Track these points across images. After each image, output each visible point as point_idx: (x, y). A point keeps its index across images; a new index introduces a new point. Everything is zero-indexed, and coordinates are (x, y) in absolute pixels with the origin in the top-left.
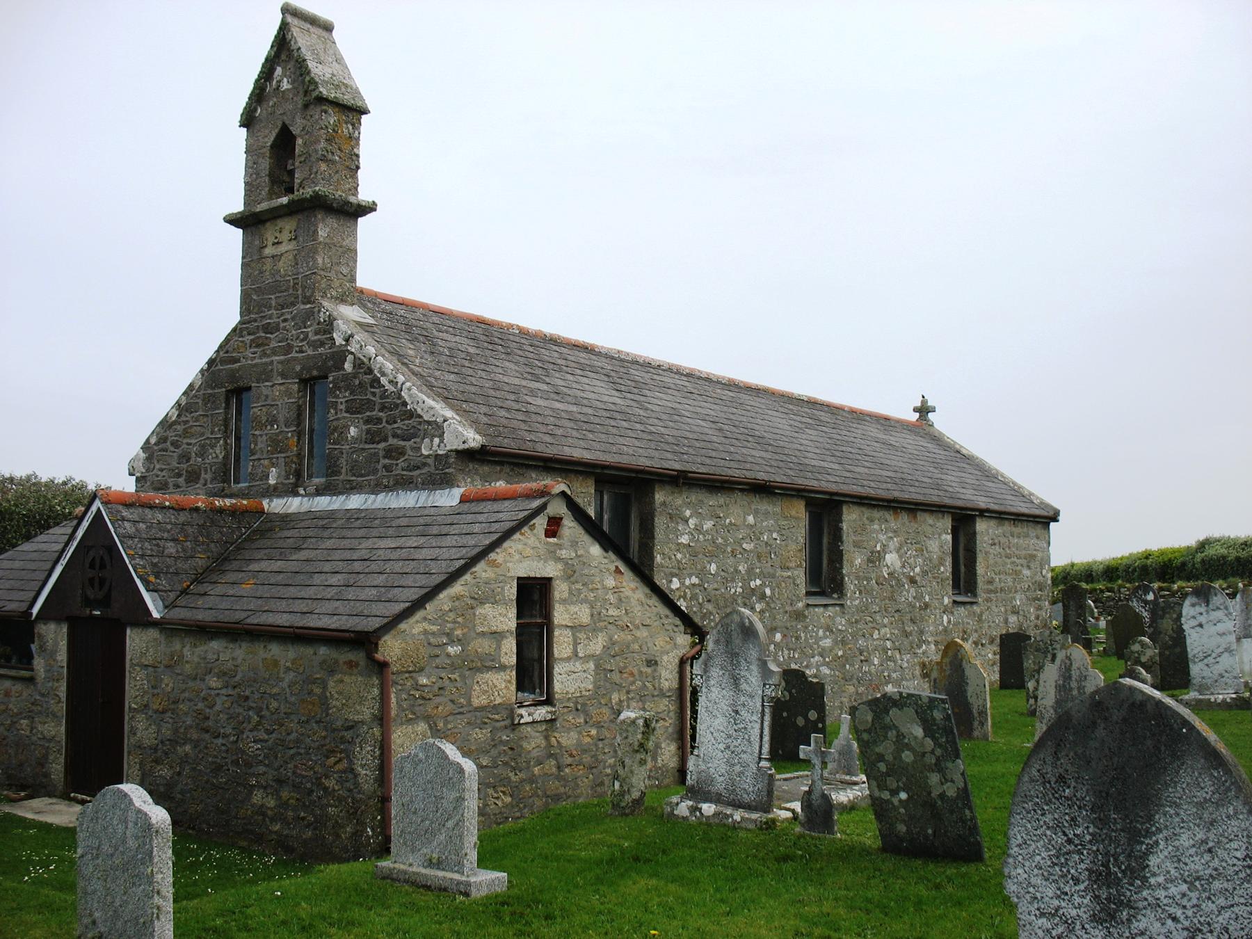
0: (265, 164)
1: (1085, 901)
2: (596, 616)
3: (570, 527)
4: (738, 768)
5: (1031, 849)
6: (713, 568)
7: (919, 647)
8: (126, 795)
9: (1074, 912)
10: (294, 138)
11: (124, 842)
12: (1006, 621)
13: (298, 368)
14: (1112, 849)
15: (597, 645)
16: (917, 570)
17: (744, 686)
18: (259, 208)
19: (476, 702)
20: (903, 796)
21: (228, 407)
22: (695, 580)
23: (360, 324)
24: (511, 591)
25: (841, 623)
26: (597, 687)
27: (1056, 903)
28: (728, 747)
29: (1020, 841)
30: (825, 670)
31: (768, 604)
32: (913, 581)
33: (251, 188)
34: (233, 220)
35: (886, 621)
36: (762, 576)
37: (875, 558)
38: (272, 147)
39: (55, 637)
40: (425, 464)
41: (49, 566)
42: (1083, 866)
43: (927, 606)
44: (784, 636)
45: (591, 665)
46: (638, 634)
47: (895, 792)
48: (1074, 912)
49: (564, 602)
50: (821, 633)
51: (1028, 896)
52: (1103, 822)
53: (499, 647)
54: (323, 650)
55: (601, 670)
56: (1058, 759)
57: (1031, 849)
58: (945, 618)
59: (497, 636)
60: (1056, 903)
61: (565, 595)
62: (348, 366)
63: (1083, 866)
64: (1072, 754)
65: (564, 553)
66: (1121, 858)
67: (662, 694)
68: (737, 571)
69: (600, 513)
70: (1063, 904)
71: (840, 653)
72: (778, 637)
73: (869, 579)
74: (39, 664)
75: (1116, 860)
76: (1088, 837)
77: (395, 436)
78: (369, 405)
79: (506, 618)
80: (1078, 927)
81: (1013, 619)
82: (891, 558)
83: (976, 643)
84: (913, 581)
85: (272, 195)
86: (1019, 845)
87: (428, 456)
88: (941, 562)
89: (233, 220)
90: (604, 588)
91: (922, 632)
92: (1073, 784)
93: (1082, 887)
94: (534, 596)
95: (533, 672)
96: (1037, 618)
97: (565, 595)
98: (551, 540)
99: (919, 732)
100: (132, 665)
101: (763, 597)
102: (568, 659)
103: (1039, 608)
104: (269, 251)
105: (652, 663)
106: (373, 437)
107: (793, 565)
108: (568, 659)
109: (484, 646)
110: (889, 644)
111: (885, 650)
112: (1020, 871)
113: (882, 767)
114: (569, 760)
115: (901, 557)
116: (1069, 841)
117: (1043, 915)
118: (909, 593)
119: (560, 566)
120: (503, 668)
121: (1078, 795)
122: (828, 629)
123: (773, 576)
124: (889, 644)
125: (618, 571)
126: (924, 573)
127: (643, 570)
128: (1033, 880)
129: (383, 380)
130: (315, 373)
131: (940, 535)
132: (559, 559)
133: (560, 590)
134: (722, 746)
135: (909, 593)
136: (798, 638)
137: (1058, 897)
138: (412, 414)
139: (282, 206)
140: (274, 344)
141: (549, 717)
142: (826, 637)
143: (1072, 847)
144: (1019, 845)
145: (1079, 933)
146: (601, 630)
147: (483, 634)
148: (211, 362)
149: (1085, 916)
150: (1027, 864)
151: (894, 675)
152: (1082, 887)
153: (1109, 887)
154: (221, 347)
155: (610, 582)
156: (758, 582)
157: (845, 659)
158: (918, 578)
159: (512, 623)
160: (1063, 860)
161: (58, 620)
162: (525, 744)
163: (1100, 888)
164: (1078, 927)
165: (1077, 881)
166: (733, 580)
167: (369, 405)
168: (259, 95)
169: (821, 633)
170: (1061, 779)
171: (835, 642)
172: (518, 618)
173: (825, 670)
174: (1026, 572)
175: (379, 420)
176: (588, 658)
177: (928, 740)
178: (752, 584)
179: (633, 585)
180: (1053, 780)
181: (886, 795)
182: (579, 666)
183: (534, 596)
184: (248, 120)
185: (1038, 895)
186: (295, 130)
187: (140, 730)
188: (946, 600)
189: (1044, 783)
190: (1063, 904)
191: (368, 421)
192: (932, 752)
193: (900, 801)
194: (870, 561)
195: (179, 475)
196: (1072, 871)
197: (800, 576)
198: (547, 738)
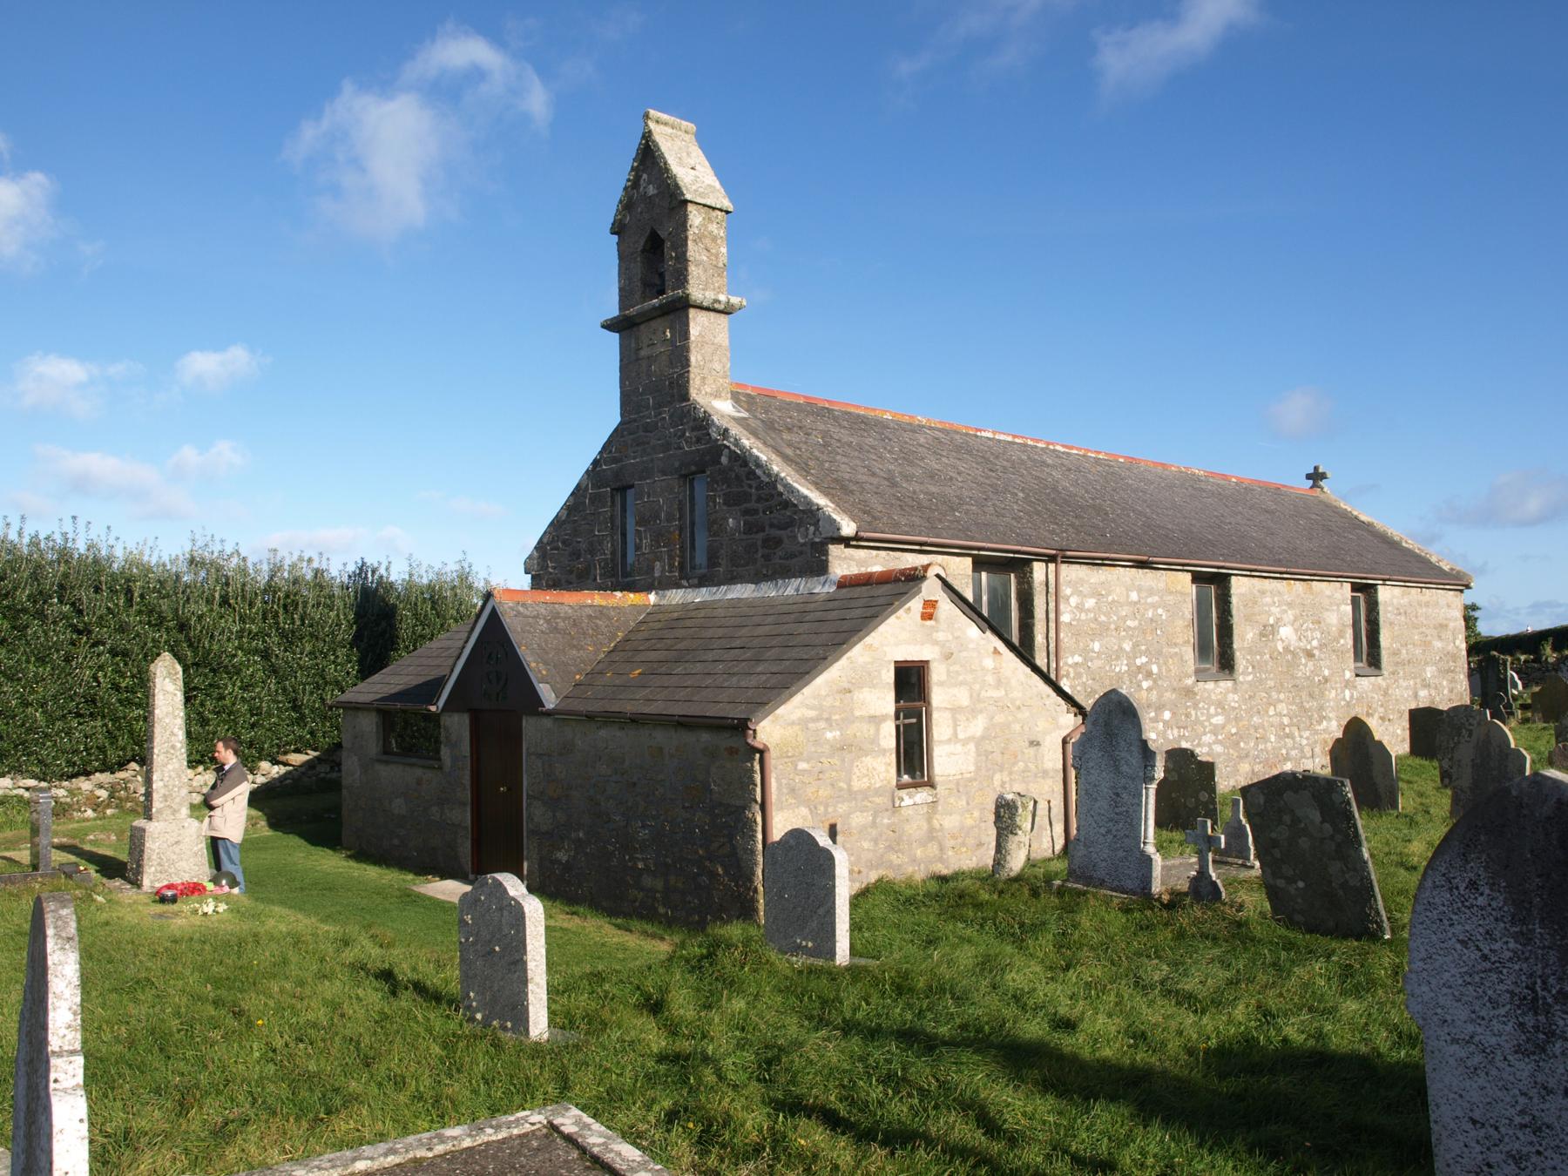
0: (637, 268)
1: (1508, 1028)
2: (976, 698)
3: (946, 607)
4: (1121, 854)
5: (1437, 965)
6: (1096, 646)
7: (1320, 723)
8: (501, 884)
9: (1493, 1040)
10: (663, 241)
11: (500, 930)
12: (1416, 696)
13: (677, 464)
14: (1539, 969)
15: (977, 726)
16: (1315, 643)
17: (1124, 768)
18: (632, 311)
19: (857, 785)
20: (1301, 884)
21: (613, 502)
22: (1077, 659)
23: (734, 419)
24: (889, 676)
25: (1233, 698)
26: (978, 768)
27: (1470, 1028)
28: (1109, 831)
29: (1423, 954)
30: (1218, 749)
31: (1155, 681)
32: (1310, 655)
33: (625, 297)
34: (610, 326)
35: (1282, 696)
36: (1147, 653)
37: (1268, 632)
38: (643, 251)
39: (458, 726)
40: (801, 553)
41: (451, 662)
42: (1502, 987)
43: (1326, 680)
44: (1174, 714)
45: (972, 746)
46: (1019, 716)
47: (1291, 880)
48: (1493, 1040)
49: (941, 684)
50: (1212, 710)
51: (1435, 1018)
52: (1525, 938)
53: (878, 730)
54: (705, 737)
55: (983, 754)
56: (1467, 862)
57: (1437, 965)
58: (1347, 693)
59: (876, 720)
60: (1470, 1028)
61: (944, 677)
62: (724, 460)
63: (1502, 987)
64: (1484, 857)
65: (940, 636)
66: (1551, 980)
67: (1045, 773)
68: (1121, 648)
69: (978, 596)
70: (1479, 1030)
71: (1234, 731)
72: (1167, 715)
73: (1262, 654)
74: (445, 752)
75: (1544, 983)
76: (1508, 954)
77: (772, 525)
78: (746, 497)
79: (884, 701)
80: (1499, 1057)
81: (1423, 693)
82: (1286, 632)
83: (1382, 718)
84: (1310, 655)
85: (645, 298)
86: (1423, 960)
87: (803, 545)
88: (1341, 634)
89: (610, 326)
90: (983, 669)
91: (1321, 708)
92: (1487, 891)
93: (1502, 1011)
94: (911, 682)
95: (912, 754)
96: (1451, 691)
97: (944, 677)
98: (929, 623)
99: (1316, 816)
100: (529, 755)
101: (1149, 674)
102: (949, 741)
103: (1453, 681)
104: (643, 353)
105: (1035, 744)
106: (750, 528)
107: (1180, 641)
108: (949, 741)
109: (866, 730)
110: (1286, 721)
111: (1282, 726)
112: (1425, 988)
113: (1277, 853)
114: (952, 843)
115: (1296, 631)
116: (1485, 958)
117: (1455, 1041)
118: (1306, 667)
119: (937, 649)
120: (884, 752)
121: (1494, 904)
122: (1220, 705)
123: (1160, 653)
124: (1286, 721)
125: (996, 651)
126: (1322, 646)
127: (1024, 651)
128: (1442, 1001)
129: (758, 472)
130: (693, 468)
131: (1338, 605)
132: (936, 643)
133: (937, 675)
134: (1103, 831)
135: (1306, 667)
136: (1188, 715)
137: (1472, 1021)
138: (787, 504)
139: (654, 308)
140: (653, 442)
141: (930, 799)
142: (1217, 714)
143: (1488, 965)
144: (1423, 960)
145: (1499, 1064)
146: (981, 712)
147: (862, 717)
148: (596, 463)
149: (1507, 1046)
150: (1434, 982)
151: (1293, 753)
152: (1502, 1011)
153: (1536, 1014)
154: (604, 447)
155: (989, 663)
156: (1144, 659)
157: (1240, 736)
158: (1316, 652)
159: (890, 707)
160: (1477, 979)
161: (458, 711)
162: (907, 827)
163: (1524, 1014)
164: (1499, 1057)
165: (1495, 1004)
166: (1118, 658)
167: (746, 497)
168: (627, 205)
169: (1212, 710)
170: (1473, 885)
171: (1228, 720)
172: (897, 701)
173: (1218, 749)
174: (1438, 644)
175: (756, 512)
176: (965, 742)
177: (1327, 826)
178: (1138, 662)
179: (1386, 612)
180: (1462, 887)
181: (1281, 883)
182: (959, 748)
183: (911, 682)
184: (618, 229)
185: (1448, 1018)
186: (663, 234)
187: (534, 815)
188: (1348, 675)
189: (1451, 889)
190: (1479, 1030)
191: (746, 512)
192: (1332, 838)
193: (1297, 889)
194: (1262, 635)
195: (571, 572)
196: (1490, 992)
197: (1189, 654)
198: (929, 820)
